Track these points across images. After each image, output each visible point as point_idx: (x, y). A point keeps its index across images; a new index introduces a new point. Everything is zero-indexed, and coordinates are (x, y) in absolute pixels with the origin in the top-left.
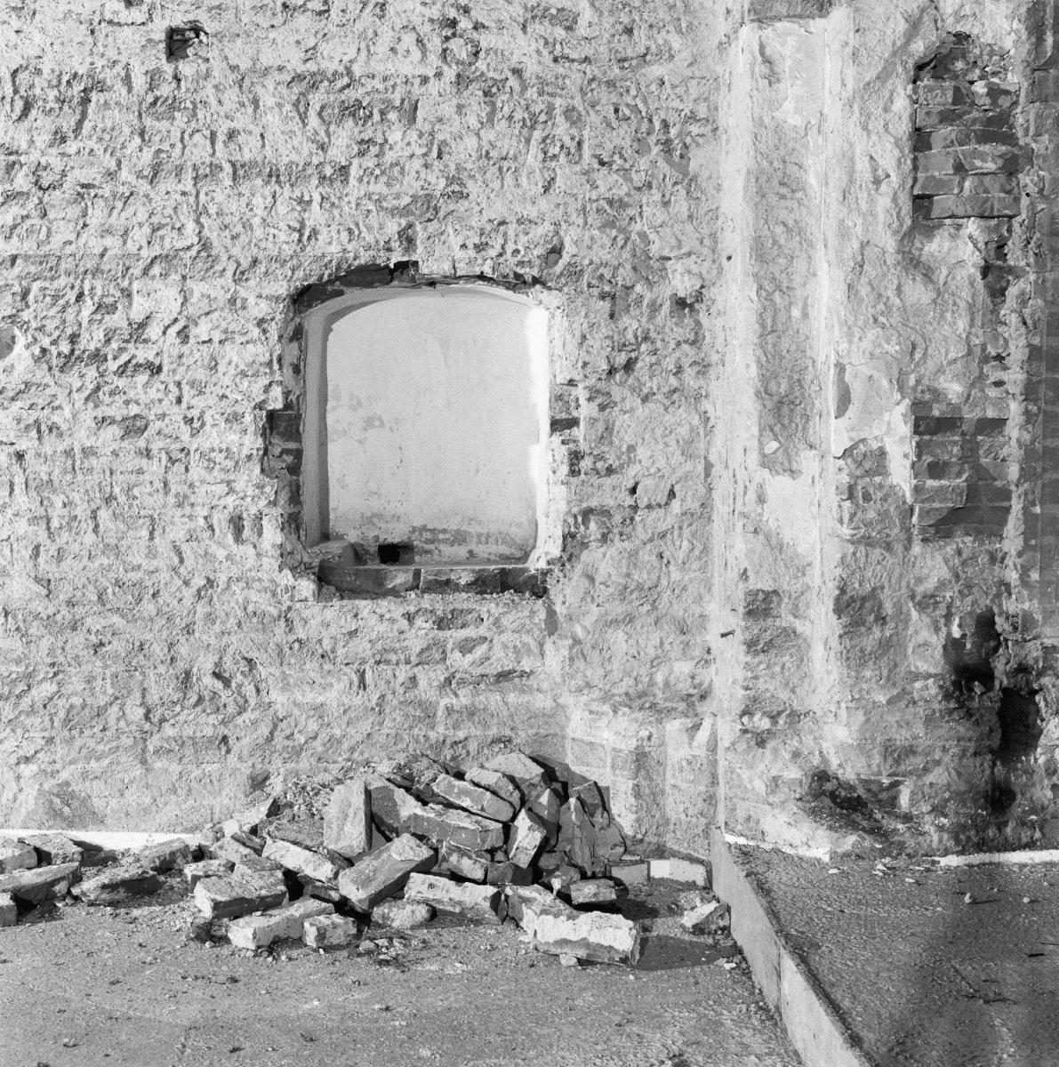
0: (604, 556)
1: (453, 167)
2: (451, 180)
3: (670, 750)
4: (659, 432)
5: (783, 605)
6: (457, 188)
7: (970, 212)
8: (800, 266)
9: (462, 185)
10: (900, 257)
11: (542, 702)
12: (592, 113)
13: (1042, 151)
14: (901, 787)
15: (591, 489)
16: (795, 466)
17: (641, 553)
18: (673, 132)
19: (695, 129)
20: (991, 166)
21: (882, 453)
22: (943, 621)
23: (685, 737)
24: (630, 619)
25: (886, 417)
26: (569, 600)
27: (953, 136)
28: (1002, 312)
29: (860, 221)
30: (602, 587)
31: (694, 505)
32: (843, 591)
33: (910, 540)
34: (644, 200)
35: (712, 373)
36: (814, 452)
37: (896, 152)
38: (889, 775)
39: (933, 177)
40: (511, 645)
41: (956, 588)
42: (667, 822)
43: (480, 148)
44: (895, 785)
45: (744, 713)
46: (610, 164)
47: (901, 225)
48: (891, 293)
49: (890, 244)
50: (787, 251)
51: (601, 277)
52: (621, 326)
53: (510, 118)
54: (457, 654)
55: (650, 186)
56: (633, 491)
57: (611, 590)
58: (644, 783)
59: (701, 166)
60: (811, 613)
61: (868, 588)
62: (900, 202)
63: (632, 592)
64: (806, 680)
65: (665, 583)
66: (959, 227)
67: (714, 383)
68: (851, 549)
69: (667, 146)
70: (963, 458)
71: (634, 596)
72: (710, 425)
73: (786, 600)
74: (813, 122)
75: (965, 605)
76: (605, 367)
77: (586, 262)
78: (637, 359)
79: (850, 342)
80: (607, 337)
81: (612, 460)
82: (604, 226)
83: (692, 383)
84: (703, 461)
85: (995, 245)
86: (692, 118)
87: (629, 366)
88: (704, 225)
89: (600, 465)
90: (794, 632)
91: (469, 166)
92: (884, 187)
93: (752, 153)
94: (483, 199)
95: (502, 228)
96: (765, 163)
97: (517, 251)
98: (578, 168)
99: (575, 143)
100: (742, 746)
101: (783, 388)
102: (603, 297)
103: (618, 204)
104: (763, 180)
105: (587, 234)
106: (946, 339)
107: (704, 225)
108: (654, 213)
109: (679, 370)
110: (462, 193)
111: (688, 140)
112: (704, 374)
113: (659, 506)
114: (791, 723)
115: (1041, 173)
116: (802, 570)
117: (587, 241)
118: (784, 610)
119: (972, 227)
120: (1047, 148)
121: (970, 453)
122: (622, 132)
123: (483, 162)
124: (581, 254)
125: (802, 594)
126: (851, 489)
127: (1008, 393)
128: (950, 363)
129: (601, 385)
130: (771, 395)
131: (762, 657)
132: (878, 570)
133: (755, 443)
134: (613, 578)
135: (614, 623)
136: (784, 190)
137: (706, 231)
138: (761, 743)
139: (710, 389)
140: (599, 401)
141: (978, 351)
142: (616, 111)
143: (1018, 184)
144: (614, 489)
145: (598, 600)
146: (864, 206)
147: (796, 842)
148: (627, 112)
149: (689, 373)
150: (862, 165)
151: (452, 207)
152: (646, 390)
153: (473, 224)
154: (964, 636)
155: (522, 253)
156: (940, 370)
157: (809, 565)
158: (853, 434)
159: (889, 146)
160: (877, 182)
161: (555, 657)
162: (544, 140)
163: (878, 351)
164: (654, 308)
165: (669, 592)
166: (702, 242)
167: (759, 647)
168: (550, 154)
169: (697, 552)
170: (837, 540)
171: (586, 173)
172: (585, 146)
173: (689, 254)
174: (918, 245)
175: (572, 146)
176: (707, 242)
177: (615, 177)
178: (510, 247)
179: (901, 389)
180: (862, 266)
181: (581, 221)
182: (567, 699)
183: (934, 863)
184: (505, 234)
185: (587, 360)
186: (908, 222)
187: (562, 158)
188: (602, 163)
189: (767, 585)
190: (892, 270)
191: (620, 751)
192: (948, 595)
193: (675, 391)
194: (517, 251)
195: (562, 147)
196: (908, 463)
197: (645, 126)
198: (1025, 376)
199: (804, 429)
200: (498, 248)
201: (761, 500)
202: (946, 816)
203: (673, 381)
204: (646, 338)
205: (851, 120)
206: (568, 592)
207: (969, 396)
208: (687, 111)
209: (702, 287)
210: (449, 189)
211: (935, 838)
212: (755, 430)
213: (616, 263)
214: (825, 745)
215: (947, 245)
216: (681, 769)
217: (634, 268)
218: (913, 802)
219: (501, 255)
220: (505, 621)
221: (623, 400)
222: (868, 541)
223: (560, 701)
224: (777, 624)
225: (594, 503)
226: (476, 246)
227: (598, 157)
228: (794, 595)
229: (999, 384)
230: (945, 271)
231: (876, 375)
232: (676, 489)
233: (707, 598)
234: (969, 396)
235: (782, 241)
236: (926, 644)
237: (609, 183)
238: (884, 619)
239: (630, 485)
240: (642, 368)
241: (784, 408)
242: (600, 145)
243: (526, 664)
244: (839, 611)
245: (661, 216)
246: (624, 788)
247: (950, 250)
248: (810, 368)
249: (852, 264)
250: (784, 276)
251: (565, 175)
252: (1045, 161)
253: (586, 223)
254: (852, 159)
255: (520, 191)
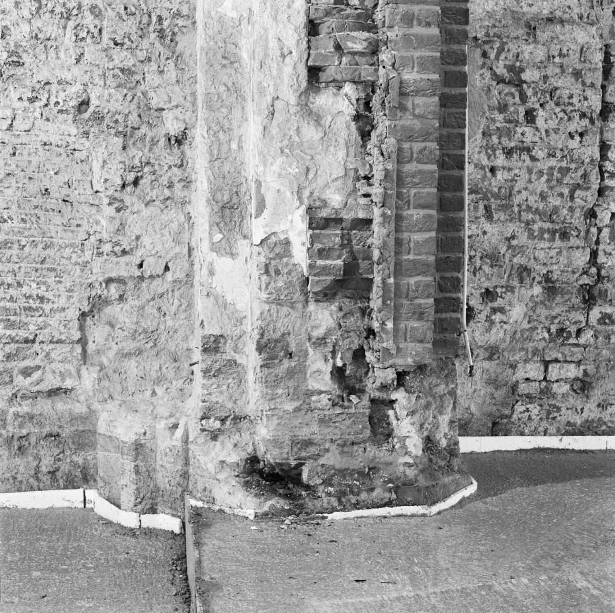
0: (122, 309)
1: (12, 44)
2: (11, 54)
3: (159, 442)
4: (157, 226)
5: (228, 345)
6: (16, 59)
7: (345, 78)
8: (236, 113)
9: (20, 57)
10: (299, 108)
11: (80, 409)
12: (109, 9)
13: (394, 37)
14: (303, 468)
15: (111, 265)
16: (234, 251)
17: (146, 308)
18: (166, 24)
19: (180, 22)
20: (359, 47)
21: (287, 243)
22: (330, 355)
23: (168, 433)
24: (139, 352)
25: (290, 217)
26: (97, 340)
27: (333, 26)
28: (369, 147)
29: (272, 83)
30: (120, 331)
31: (181, 275)
32: (262, 335)
33: (307, 302)
34: (146, 70)
35: (193, 186)
36: (247, 241)
37: (296, 36)
38: (295, 460)
39: (321, 54)
40: (57, 371)
41: (339, 333)
42: (158, 490)
43: (31, 32)
44: (301, 465)
45: (202, 418)
46: (122, 45)
47: (299, 86)
48: (292, 133)
49: (293, 100)
50: (227, 103)
51: (116, 121)
52: (131, 155)
53: (52, 11)
54: (21, 378)
55: (149, 60)
56: (141, 266)
57: (126, 333)
58: (141, 464)
59: (185, 47)
60: (246, 349)
61: (279, 334)
62: (299, 71)
63: (140, 334)
64: (244, 396)
65: (163, 328)
66: (340, 88)
67: (194, 193)
68: (267, 307)
69: (161, 34)
70: (342, 246)
71: (142, 337)
72: (191, 222)
73: (229, 341)
74: (245, 16)
75: (344, 344)
76: (119, 182)
77: (106, 111)
78: (142, 177)
79: (265, 166)
80: (121, 162)
81: (126, 245)
82: (117, 87)
83: (179, 193)
84: (187, 246)
85: (363, 101)
86: (178, 14)
87: (136, 182)
88: (187, 87)
89: (117, 249)
90: (236, 363)
91: (24, 44)
92: (288, 60)
93: (203, 36)
94: (34, 66)
95: (47, 87)
96: (212, 43)
97: (57, 103)
98: (99, 47)
99: (97, 30)
100: (201, 440)
101: (226, 198)
102: (118, 134)
103: (127, 71)
104: (211, 54)
105: (106, 92)
106: (330, 165)
107: (187, 87)
108: (153, 79)
109: (170, 186)
110: (19, 62)
111: (176, 30)
112: (187, 187)
113: (158, 276)
114: (235, 423)
115: (393, 52)
116: (240, 321)
117: (106, 97)
118: (228, 347)
119: (348, 88)
120: (397, 36)
121: (346, 242)
122: (129, 22)
123: (33, 41)
124: (102, 105)
125: (240, 337)
126: (267, 266)
127: (372, 201)
128: (333, 181)
129: (117, 195)
130: (217, 202)
131: (214, 379)
132: (286, 320)
133: (206, 235)
134: (127, 325)
135: (128, 355)
136: (225, 62)
137: (188, 91)
138: (214, 438)
139: (192, 197)
140: (116, 205)
141: (352, 173)
142: (126, 8)
143: (378, 59)
144: (127, 265)
145: (116, 340)
146: (275, 73)
147: (234, 505)
148: (133, 10)
149: (178, 186)
150: (273, 44)
151: (12, 72)
152: (148, 198)
153: (27, 84)
154: (345, 365)
155: (61, 104)
156: (327, 185)
157: (245, 317)
158: (267, 229)
159: (291, 32)
160: (283, 56)
161: (89, 377)
162: (76, 28)
163: (284, 172)
164: (154, 143)
165: (165, 334)
166: (185, 98)
167: (212, 373)
168: (80, 37)
169: (183, 307)
170: (258, 301)
171: (106, 50)
172: (104, 32)
173: (177, 106)
174: (311, 100)
175: (96, 31)
176: (189, 98)
177: (125, 53)
178: (53, 100)
179: (300, 198)
180: (273, 114)
181: (102, 83)
182: (96, 406)
183: (324, 518)
184: (49, 91)
185: (107, 177)
186: (304, 84)
187: (89, 40)
188: (116, 44)
189: (217, 332)
190: (293, 117)
191: (126, 443)
192: (334, 337)
193: (167, 199)
194: (57, 103)
195: (88, 32)
196: (305, 249)
197: (145, 20)
198: (382, 190)
199: (240, 225)
200: (44, 101)
201: (211, 273)
202: (332, 486)
203: (167, 193)
204: (148, 163)
205: (267, 12)
206: (96, 335)
207: (346, 203)
208: (174, 10)
209: (186, 129)
210: (10, 60)
211: (325, 500)
212: (207, 226)
213: (127, 111)
214: (257, 438)
215: (331, 100)
216: (166, 455)
217: (140, 116)
218: (310, 478)
219: (46, 105)
220: (53, 355)
221: (133, 205)
222: (278, 302)
223: (92, 408)
224: (224, 357)
225: (113, 275)
226: (29, 99)
227: (113, 40)
228: (235, 338)
229: (367, 195)
230: (330, 119)
231: (282, 189)
232: (170, 265)
233: (191, 338)
234: (346, 203)
235: (224, 97)
236: (319, 371)
237: (121, 57)
238: (291, 354)
239: (138, 262)
240: (145, 183)
241: (229, 212)
242: (115, 32)
243: (68, 384)
244: (260, 349)
245: (157, 80)
246: (128, 468)
247: (333, 104)
248: (244, 184)
249: (267, 113)
250: (225, 120)
251: (91, 52)
252: (395, 44)
253: (105, 84)
254: (267, 40)
255: (59, 62)
